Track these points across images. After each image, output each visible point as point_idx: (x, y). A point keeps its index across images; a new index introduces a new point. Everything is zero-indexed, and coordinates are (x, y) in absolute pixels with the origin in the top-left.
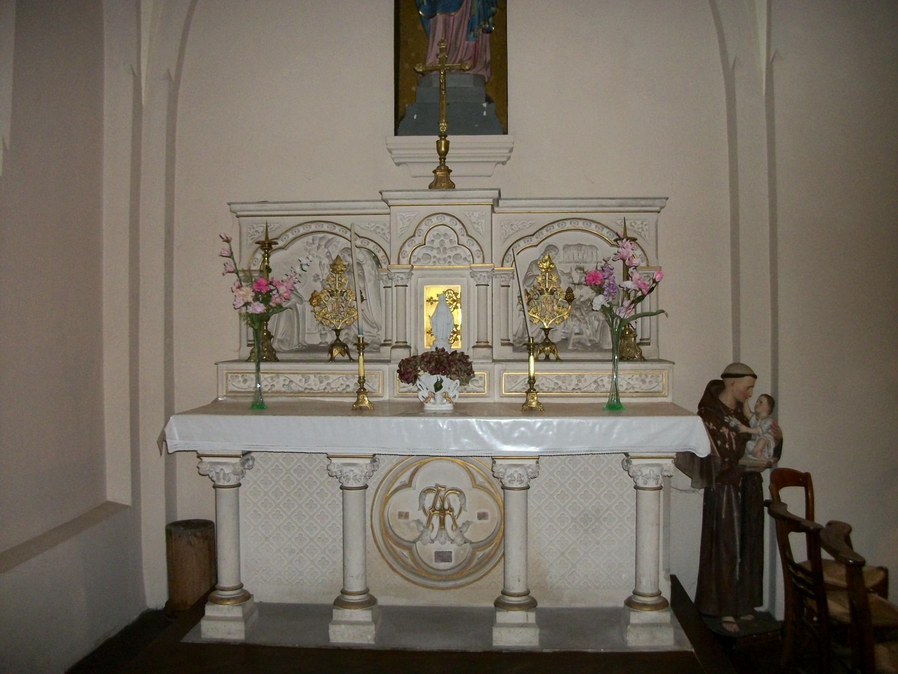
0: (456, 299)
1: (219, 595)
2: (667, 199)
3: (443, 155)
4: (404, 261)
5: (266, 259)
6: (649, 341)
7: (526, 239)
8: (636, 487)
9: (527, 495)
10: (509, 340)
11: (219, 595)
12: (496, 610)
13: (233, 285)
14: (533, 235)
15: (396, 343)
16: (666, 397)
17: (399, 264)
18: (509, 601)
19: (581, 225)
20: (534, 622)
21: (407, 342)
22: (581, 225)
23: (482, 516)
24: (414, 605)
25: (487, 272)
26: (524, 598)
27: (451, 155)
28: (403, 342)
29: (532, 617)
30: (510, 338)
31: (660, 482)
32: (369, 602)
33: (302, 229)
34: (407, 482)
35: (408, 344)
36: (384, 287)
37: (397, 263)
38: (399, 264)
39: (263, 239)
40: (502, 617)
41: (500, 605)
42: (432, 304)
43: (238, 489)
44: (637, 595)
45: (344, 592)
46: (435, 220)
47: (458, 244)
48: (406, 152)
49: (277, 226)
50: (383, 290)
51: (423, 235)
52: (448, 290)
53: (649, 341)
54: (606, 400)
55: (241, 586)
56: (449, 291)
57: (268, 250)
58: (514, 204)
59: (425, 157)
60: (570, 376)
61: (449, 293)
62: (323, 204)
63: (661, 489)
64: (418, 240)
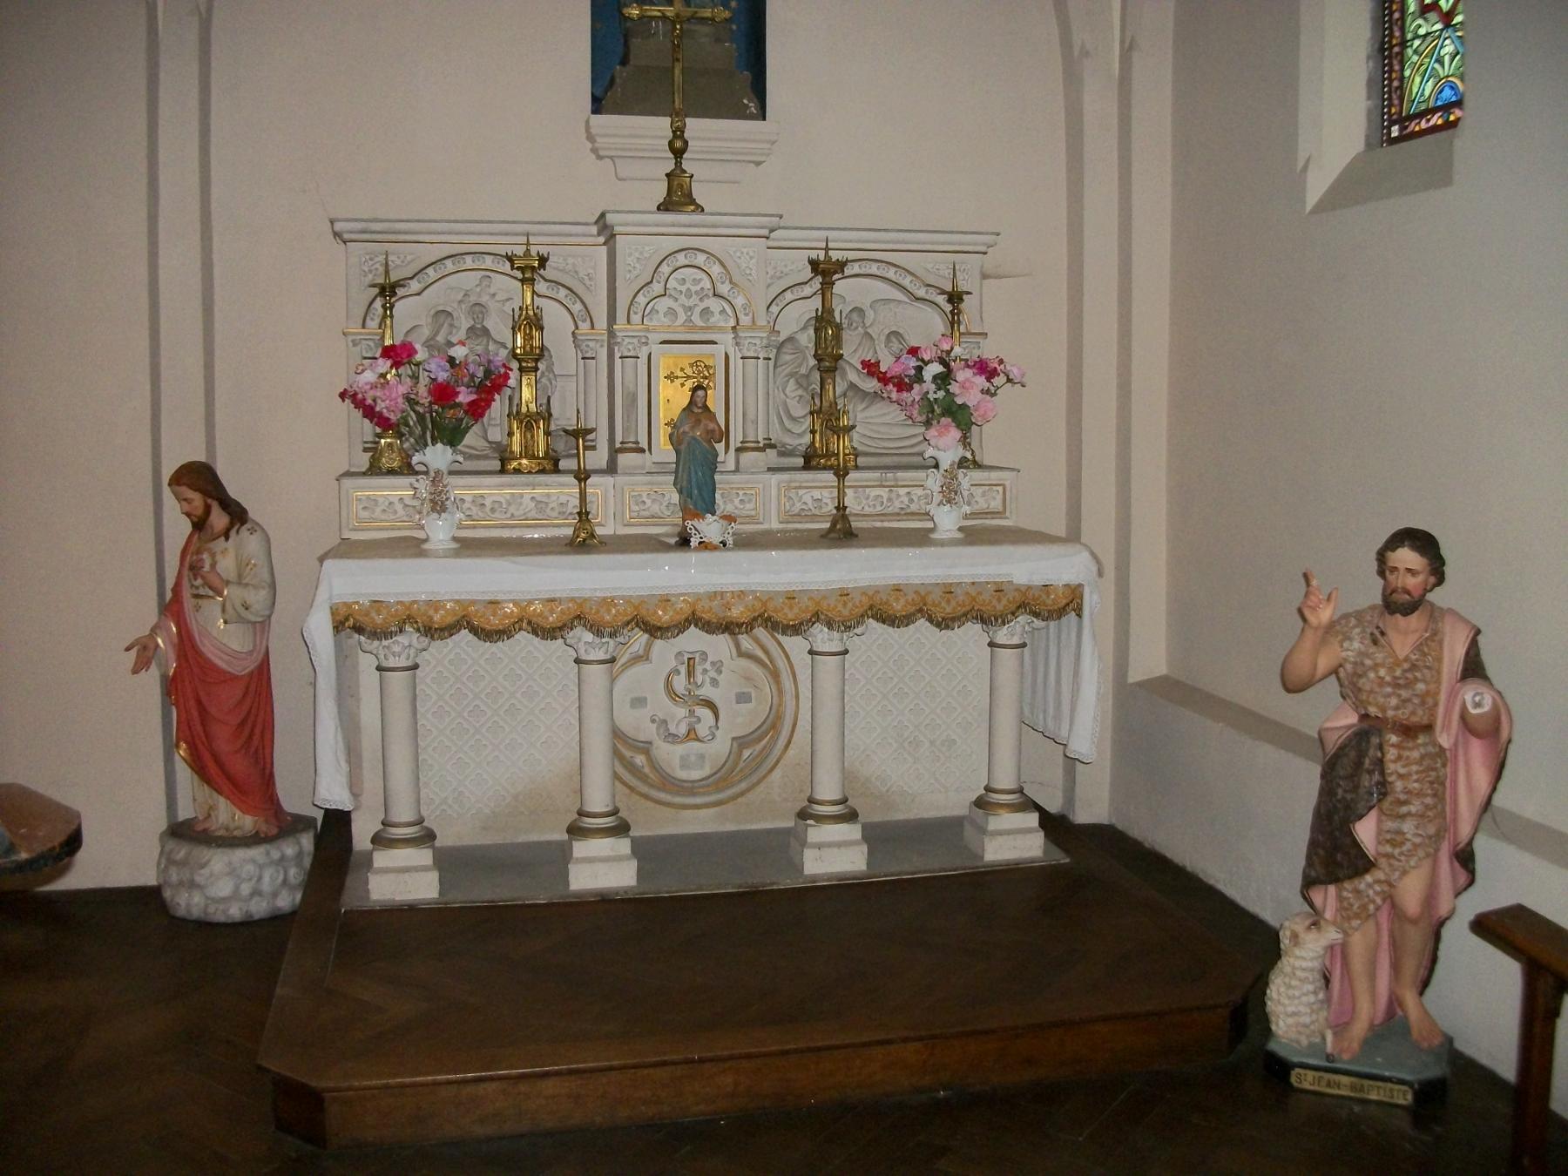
0: (707, 375)
1: (582, 822)
2: (998, 234)
3: (678, 151)
4: (636, 318)
5: (388, 312)
6: (594, 443)
7: (794, 289)
8: (578, 661)
9: (414, 676)
10: (758, 442)
11: (582, 822)
12: (374, 850)
13: (989, 351)
14: (806, 283)
15: (741, 443)
16: (762, 523)
17: (364, 327)
18: (585, 823)
19: (874, 269)
20: (630, 852)
21: (639, 443)
22: (874, 269)
23: (743, 698)
24: (939, 816)
25: (762, 338)
26: (840, 807)
27: (695, 149)
28: (634, 443)
29: (1033, 819)
30: (771, 437)
31: (611, 650)
32: (427, 837)
33: (490, 261)
34: (641, 652)
35: (773, 442)
36: (742, 358)
37: (361, 327)
38: (364, 327)
39: (381, 281)
40: (581, 848)
41: (576, 831)
42: (672, 381)
43: (1023, 651)
44: (813, 803)
45: (811, 801)
46: (681, 259)
47: (665, 295)
48: (648, 141)
49: (404, 260)
50: (618, 362)
51: (427, 281)
52: (696, 362)
53: (594, 443)
54: (569, 531)
55: (420, 821)
56: (698, 364)
57: (391, 297)
58: (472, 230)
59: (755, 154)
60: (522, 496)
61: (697, 366)
62: (547, 226)
63: (847, 653)
64: (657, 288)
